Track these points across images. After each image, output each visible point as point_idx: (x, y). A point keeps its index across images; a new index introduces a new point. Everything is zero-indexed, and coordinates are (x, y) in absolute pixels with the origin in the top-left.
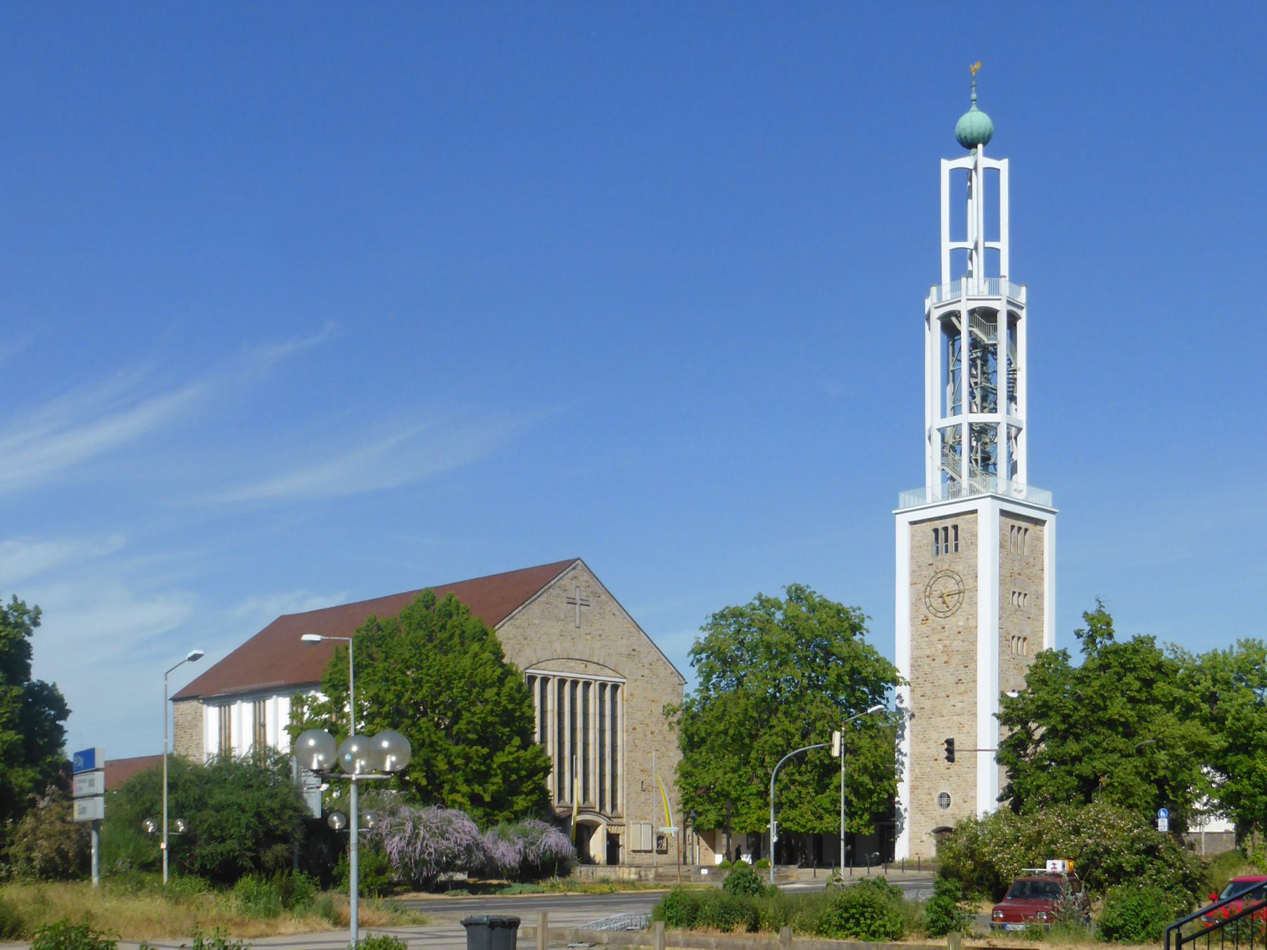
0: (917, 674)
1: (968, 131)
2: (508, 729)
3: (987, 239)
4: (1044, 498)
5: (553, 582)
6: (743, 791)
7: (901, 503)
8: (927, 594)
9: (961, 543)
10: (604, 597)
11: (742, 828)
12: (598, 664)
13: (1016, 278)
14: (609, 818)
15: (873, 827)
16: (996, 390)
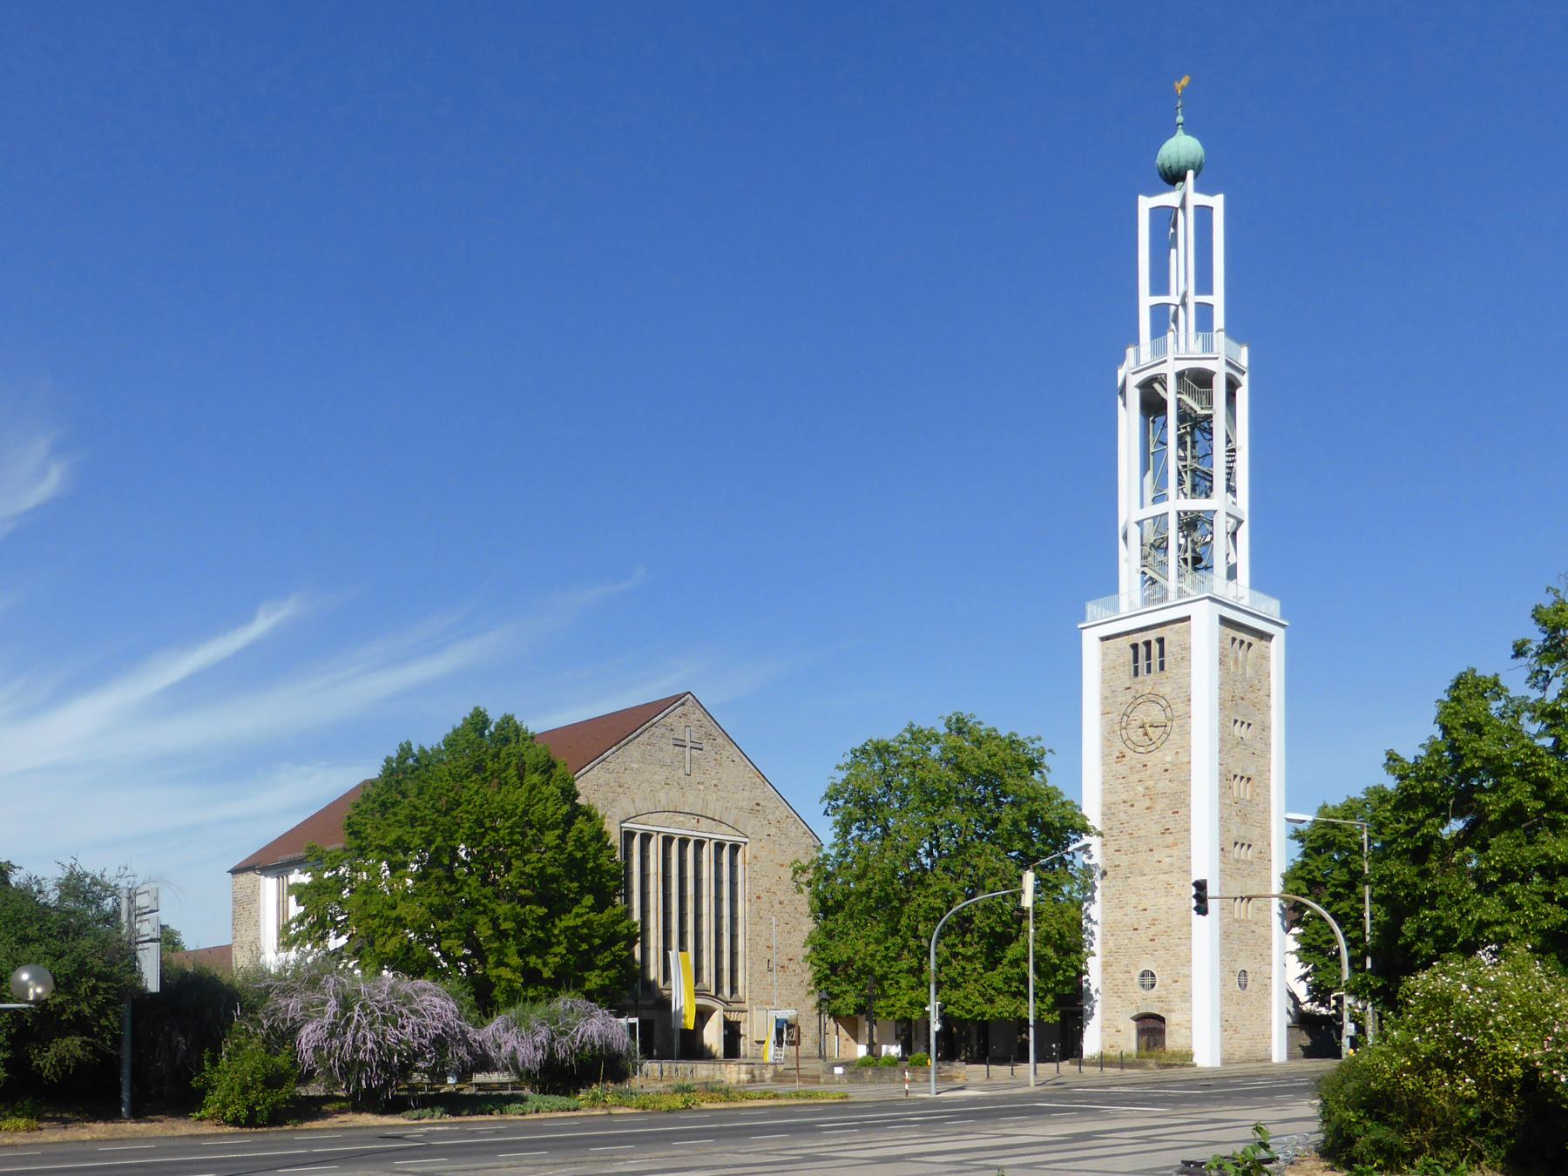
0: (1110, 824)
1: (1174, 159)
2: (576, 884)
3: (1199, 292)
4: (1272, 607)
5: (655, 719)
6: (891, 967)
7: (1089, 617)
8: (1124, 724)
9: (1168, 659)
10: (720, 740)
11: (889, 1014)
12: (714, 820)
13: (1232, 331)
14: (727, 1003)
15: (1057, 1013)
16: (1212, 476)
